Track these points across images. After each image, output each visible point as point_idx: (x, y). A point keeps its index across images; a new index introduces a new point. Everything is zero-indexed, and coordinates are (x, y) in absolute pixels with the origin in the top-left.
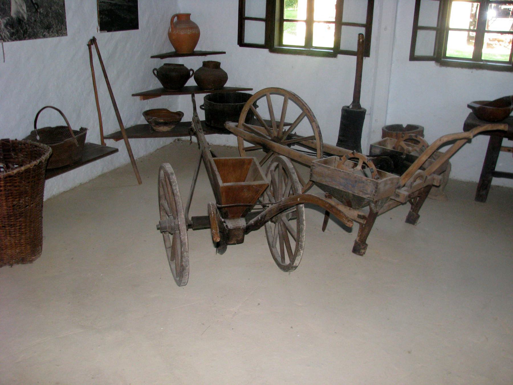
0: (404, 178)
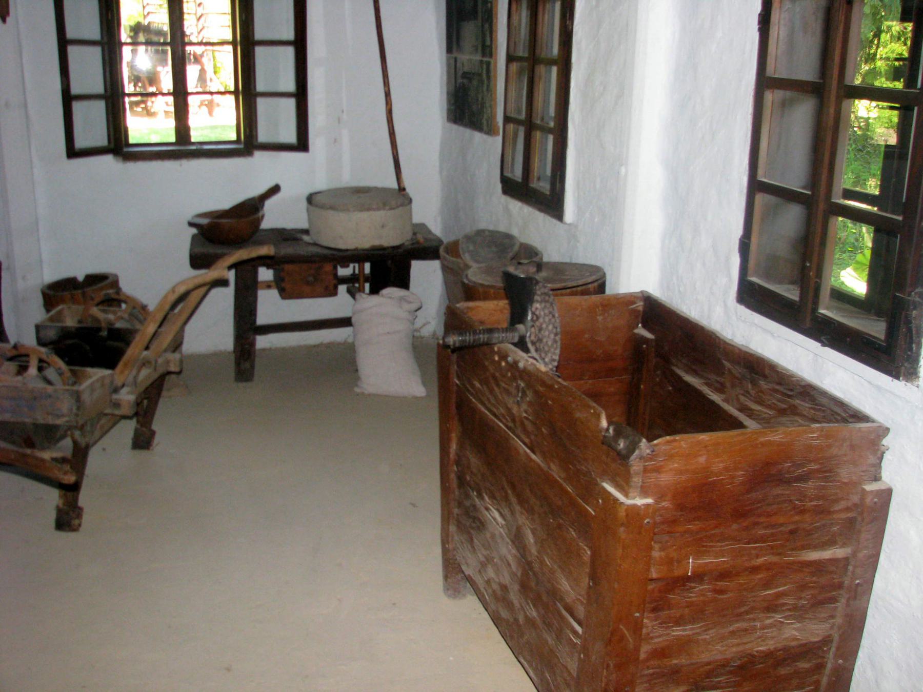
0: (122, 372)
